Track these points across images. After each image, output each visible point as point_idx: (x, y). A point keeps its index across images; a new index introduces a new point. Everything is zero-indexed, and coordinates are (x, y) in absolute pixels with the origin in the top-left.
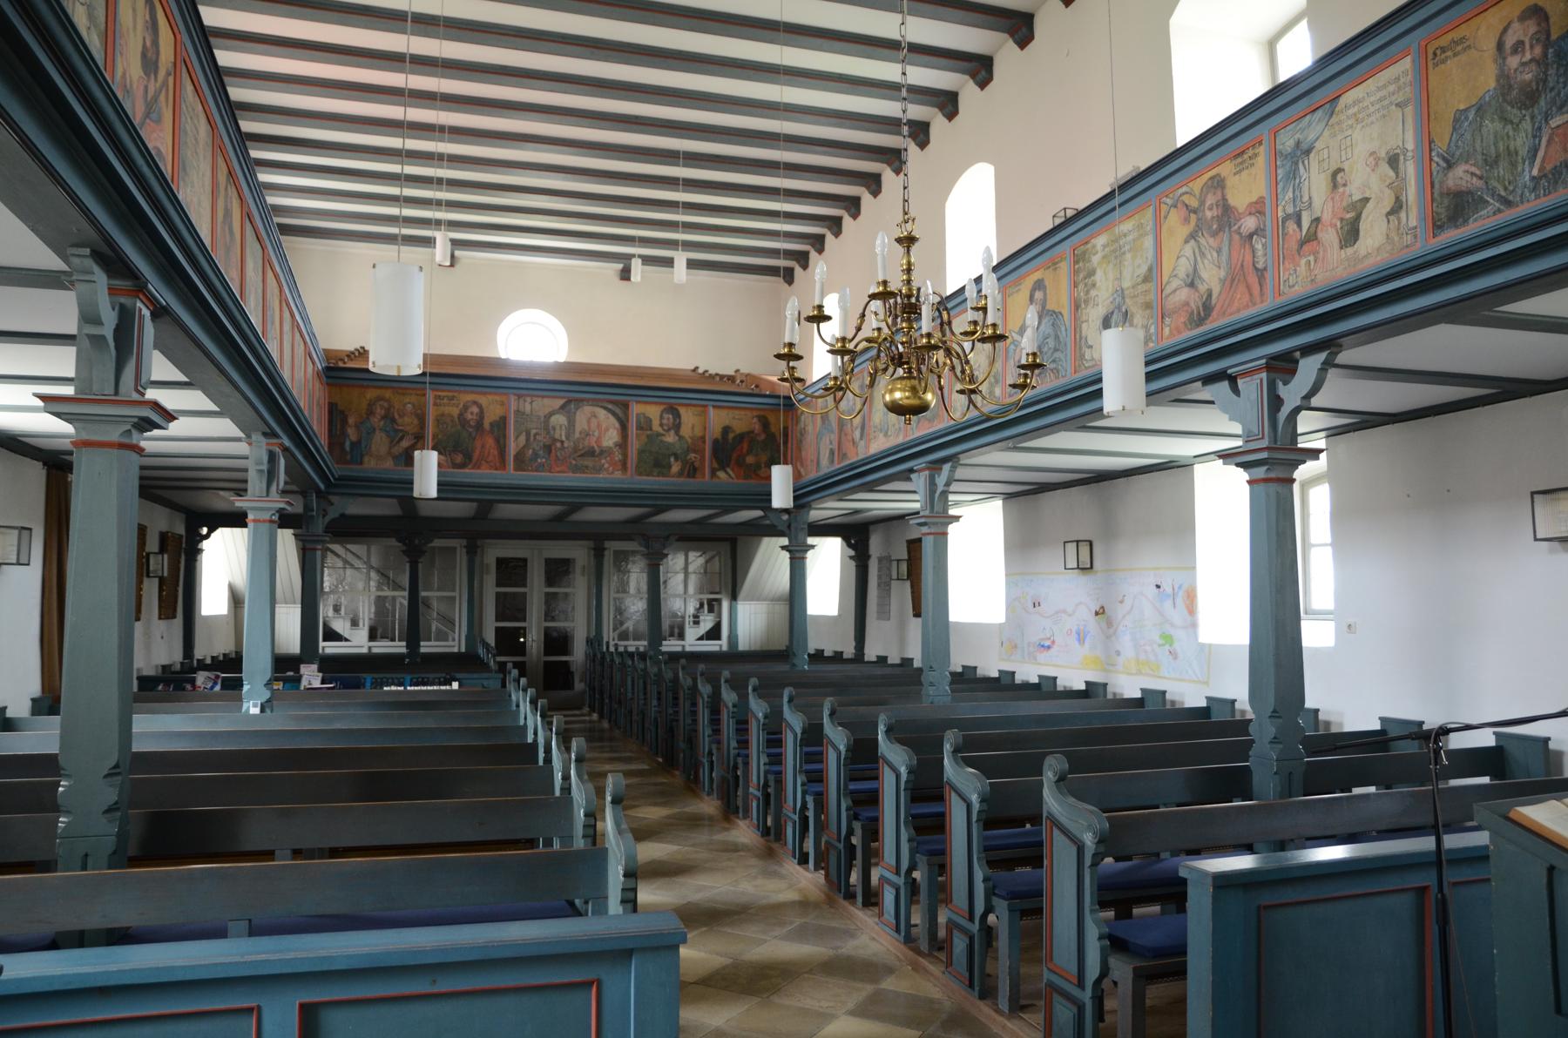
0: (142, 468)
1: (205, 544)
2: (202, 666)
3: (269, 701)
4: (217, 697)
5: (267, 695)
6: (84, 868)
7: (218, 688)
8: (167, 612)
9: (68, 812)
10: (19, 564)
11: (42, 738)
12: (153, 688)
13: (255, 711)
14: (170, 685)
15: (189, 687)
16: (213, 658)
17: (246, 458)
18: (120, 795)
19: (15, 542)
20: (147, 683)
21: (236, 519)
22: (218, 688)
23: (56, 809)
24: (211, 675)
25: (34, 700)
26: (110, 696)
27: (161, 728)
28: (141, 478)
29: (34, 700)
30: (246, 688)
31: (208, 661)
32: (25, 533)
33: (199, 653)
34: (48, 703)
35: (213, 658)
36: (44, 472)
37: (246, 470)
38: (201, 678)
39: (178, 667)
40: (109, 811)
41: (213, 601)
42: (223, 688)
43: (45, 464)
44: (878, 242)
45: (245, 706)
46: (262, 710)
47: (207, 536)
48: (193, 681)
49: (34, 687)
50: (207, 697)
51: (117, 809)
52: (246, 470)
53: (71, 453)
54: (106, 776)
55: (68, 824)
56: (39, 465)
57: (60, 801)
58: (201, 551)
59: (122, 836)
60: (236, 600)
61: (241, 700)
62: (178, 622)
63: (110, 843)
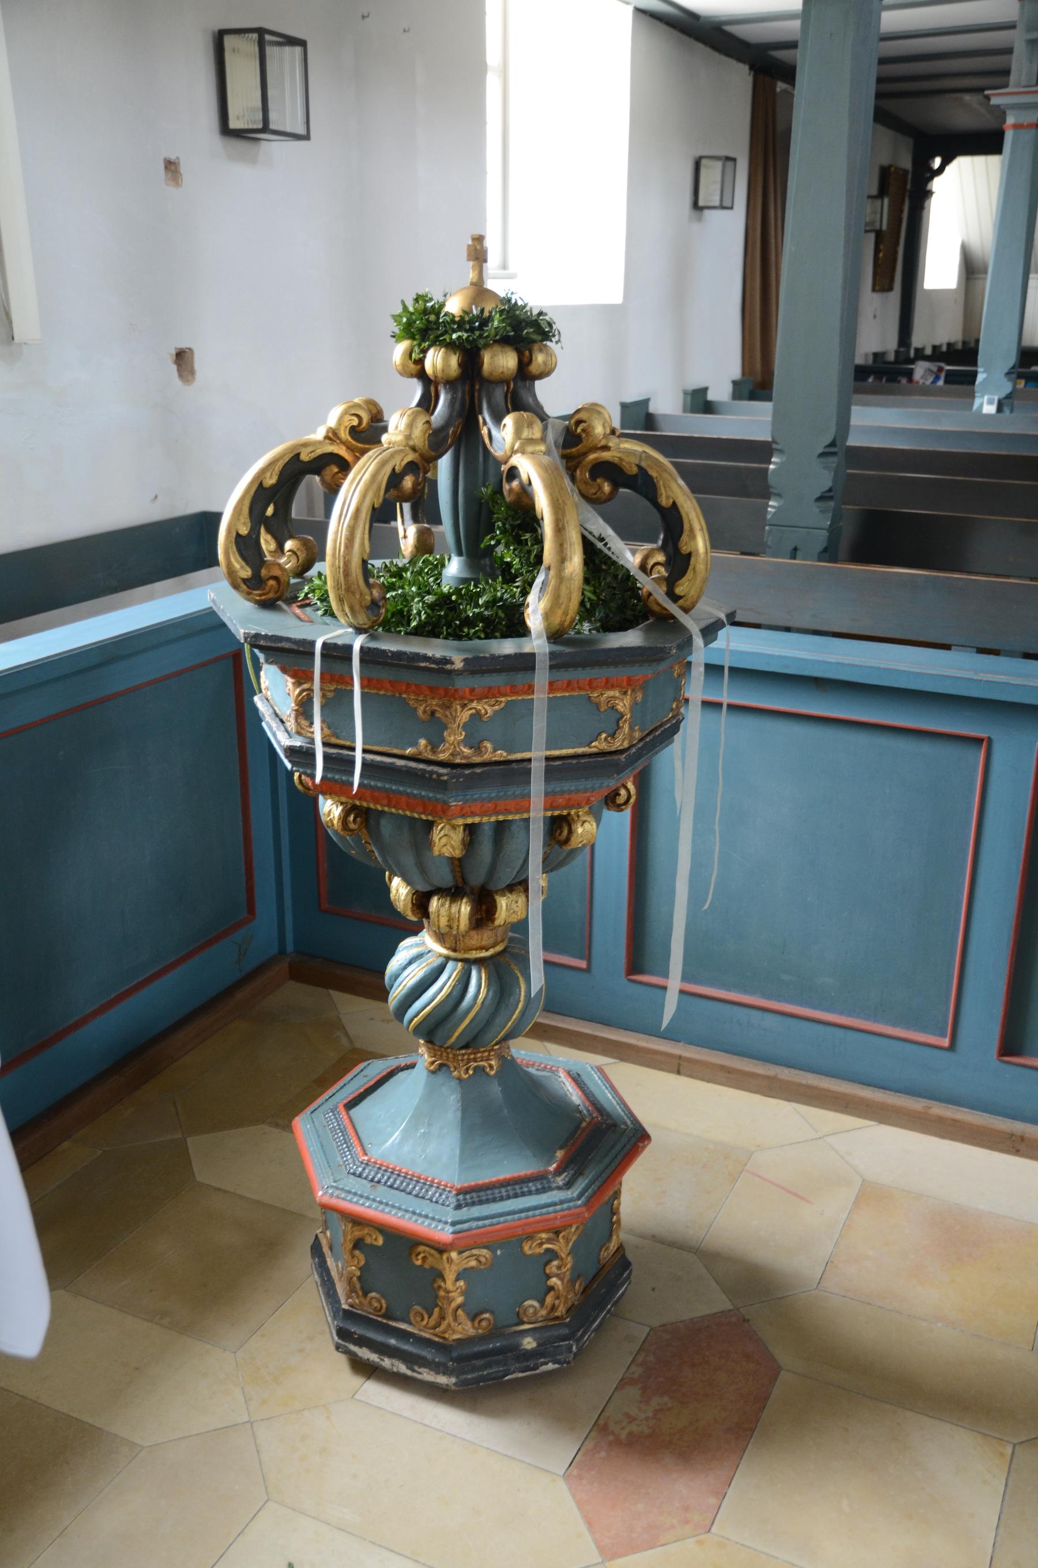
0: (882, 61)
1: (937, 184)
2: (920, 355)
3: (1009, 397)
4: (940, 392)
5: (1007, 388)
6: (793, 557)
7: (941, 383)
8: (882, 283)
9: (779, 495)
10: (722, 207)
11: (752, 422)
12: (865, 379)
13: (990, 409)
14: (884, 375)
15: (904, 381)
16: (935, 348)
17: (1011, 26)
18: (835, 481)
19: (719, 178)
20: (861, 373)
21: (986, 142)
22: (941, 383)
23: (766, 494)
24: (933, 366)
25: (735, 383)
26: (830, 373)
27: (880, 422)
28: (880, 80)
29: (735, 383)
30: (981, 377)
31: (928, 351)
32: (730, 164)
33: (919, 339)
34: (755, 384)
35: (935, 348)
36: (750, 79)
37: (1009, 51)
38: (920, 370)
39: (891, 357)
40: (821, 499)
41: (939, 272)
42: (946, 382)
43: (751, 68)
44: (262, 541)
45: (977, 402)
46: (1000, 409)
47: (941, 170)
48: (909, 374)
49: (734, 369)
50: (925, 391)
51: (831, 498)
52: (1009, 51)
53: (793, 45)
54: (822, 455)
55: (778, 509)
56: (744, 69)
57: (772, 480)
58: (929, 193)
59: (834, 532)
60: (971, 268)
61: (972, 396)
62: (895, 296)
63: (821, 538)
